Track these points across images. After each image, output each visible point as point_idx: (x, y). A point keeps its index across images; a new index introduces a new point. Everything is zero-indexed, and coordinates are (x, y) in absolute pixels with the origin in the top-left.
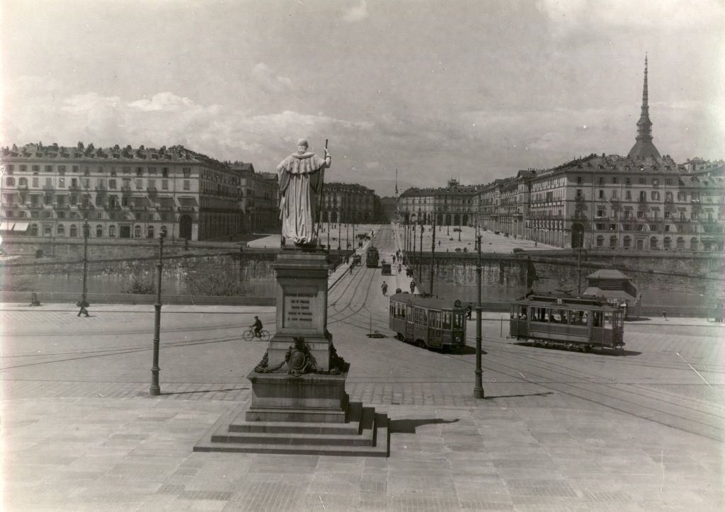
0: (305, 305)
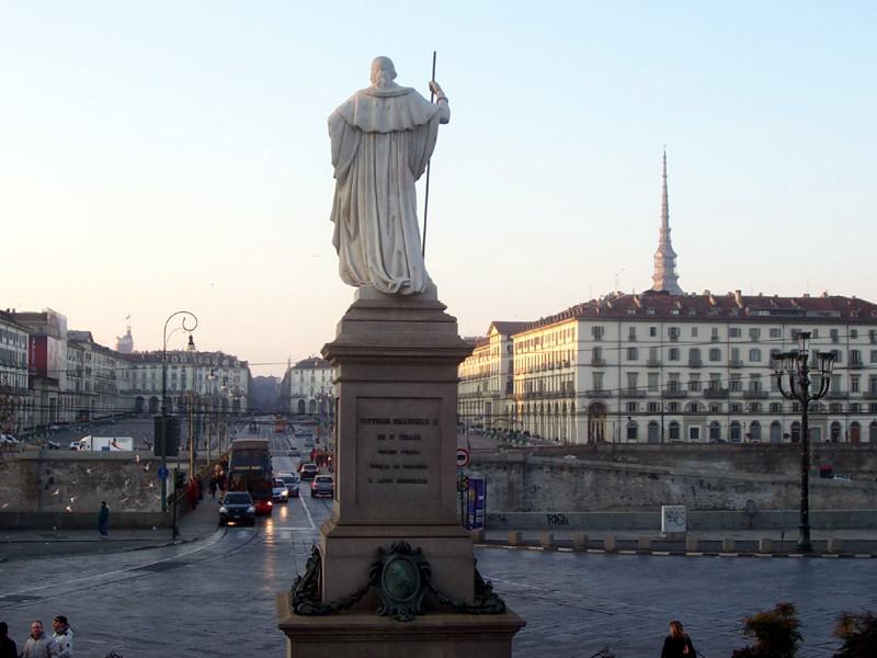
0: (410, 445)
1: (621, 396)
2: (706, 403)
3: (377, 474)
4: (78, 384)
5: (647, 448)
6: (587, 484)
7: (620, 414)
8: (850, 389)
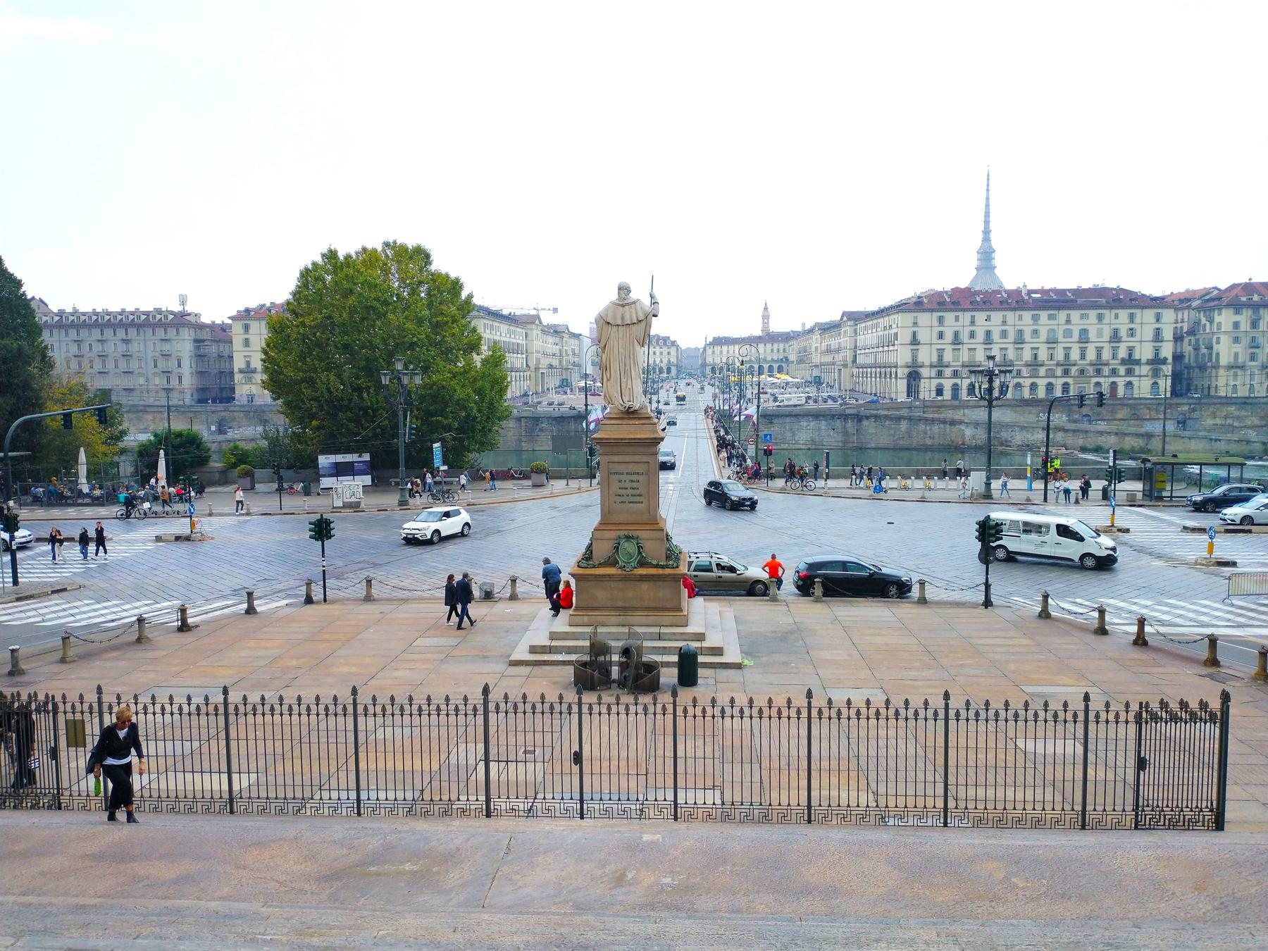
0: (635, 485)
1: (932, 366)
3: (618, 499)
4: (560, 362)
5: (949, 403)
6: (903, 429)
7: (930, 378)
8: (1111, 357)
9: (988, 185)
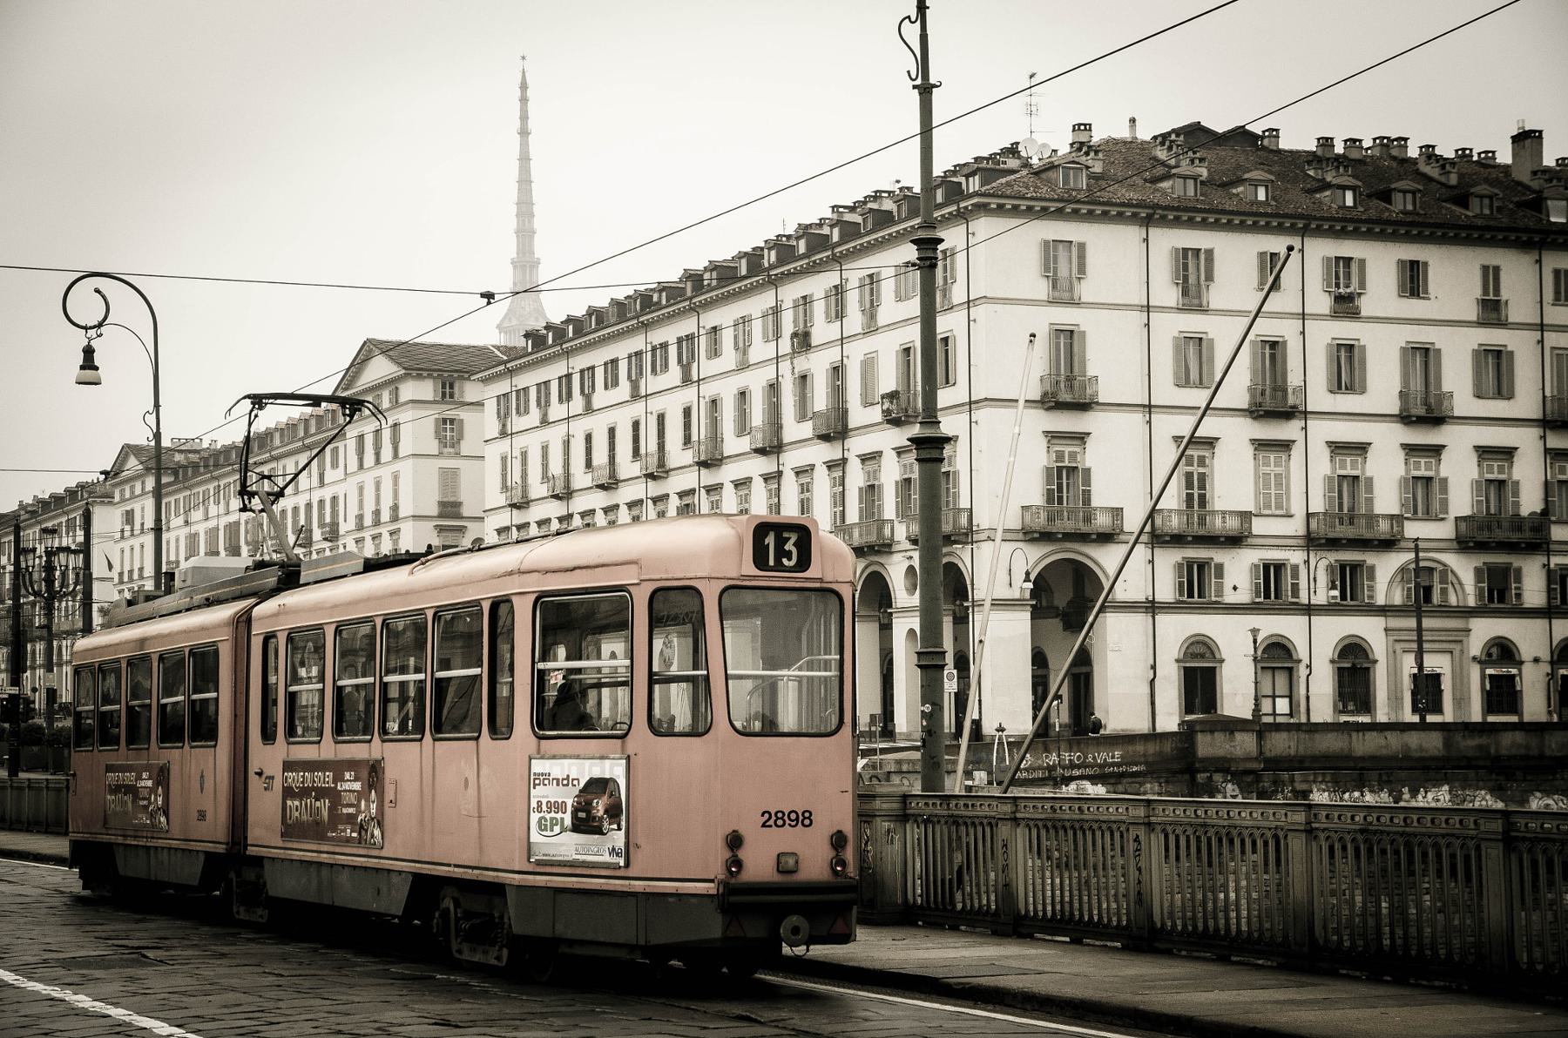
2: (1464, 569)
7: (1152, 607)
9: (524, 117)
